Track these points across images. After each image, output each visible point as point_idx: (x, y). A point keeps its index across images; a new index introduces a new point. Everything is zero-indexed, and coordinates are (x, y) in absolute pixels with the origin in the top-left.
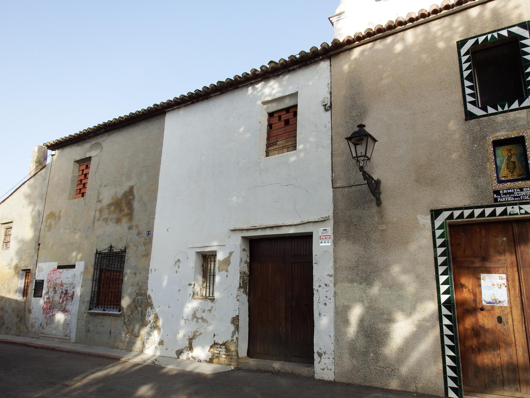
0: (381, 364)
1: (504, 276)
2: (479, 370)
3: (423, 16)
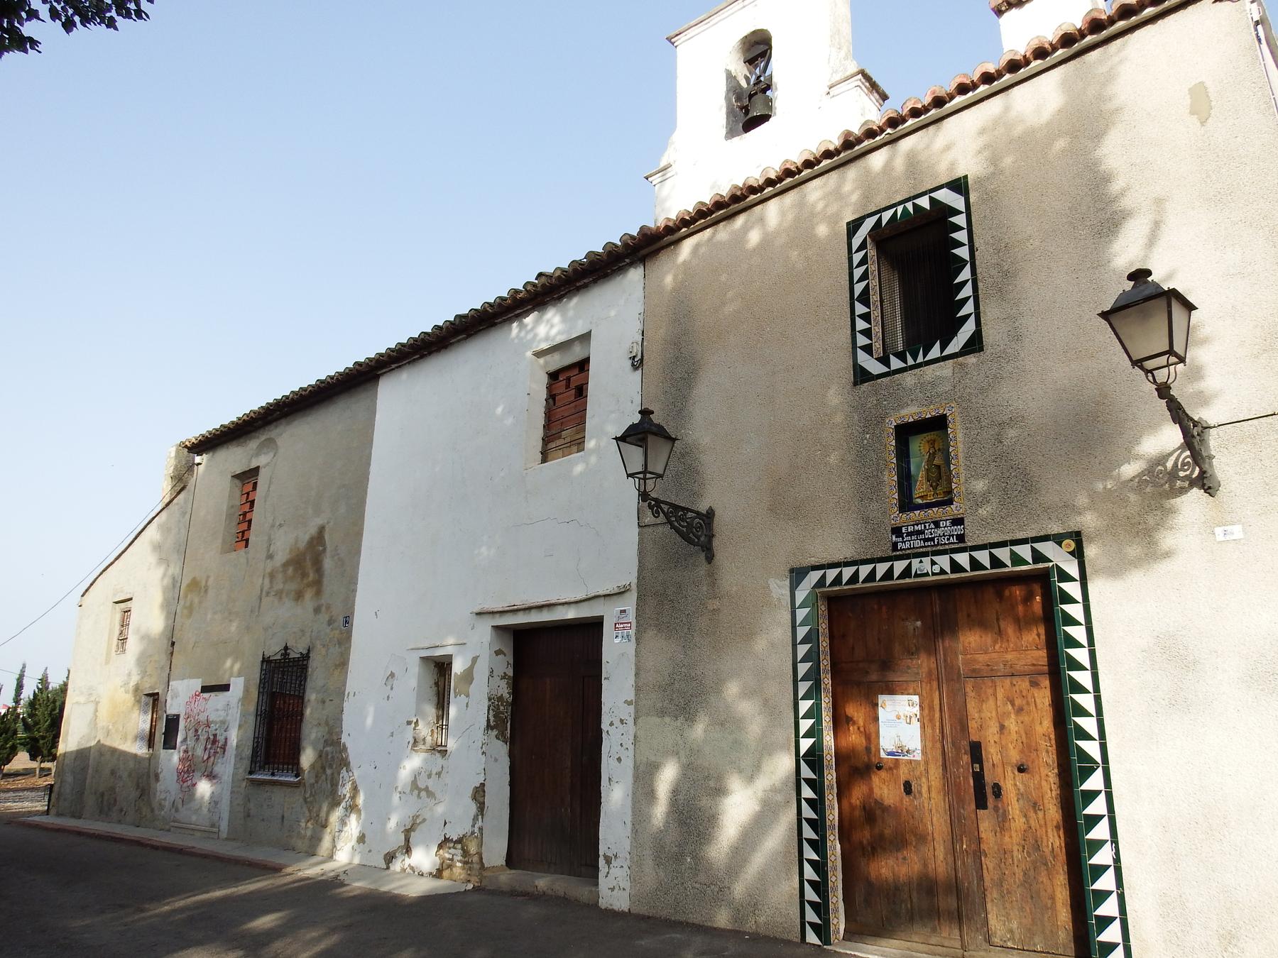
0: (702, 877)
1: (916, 698)
2: (892, 892)
3: (788, 173)
